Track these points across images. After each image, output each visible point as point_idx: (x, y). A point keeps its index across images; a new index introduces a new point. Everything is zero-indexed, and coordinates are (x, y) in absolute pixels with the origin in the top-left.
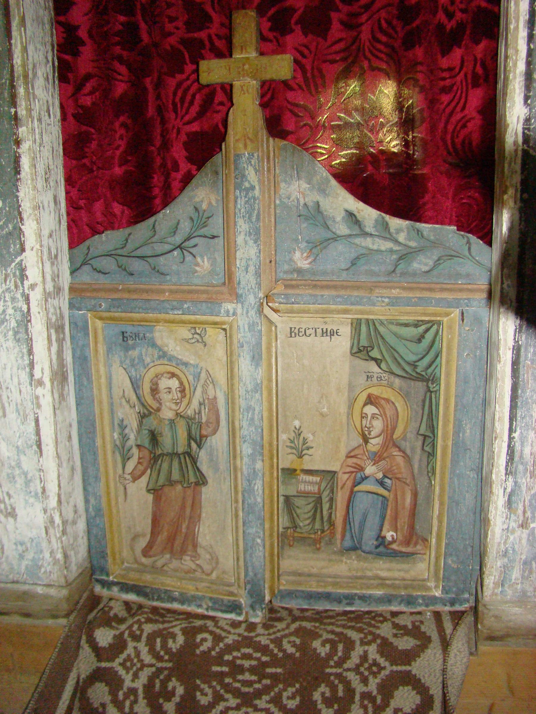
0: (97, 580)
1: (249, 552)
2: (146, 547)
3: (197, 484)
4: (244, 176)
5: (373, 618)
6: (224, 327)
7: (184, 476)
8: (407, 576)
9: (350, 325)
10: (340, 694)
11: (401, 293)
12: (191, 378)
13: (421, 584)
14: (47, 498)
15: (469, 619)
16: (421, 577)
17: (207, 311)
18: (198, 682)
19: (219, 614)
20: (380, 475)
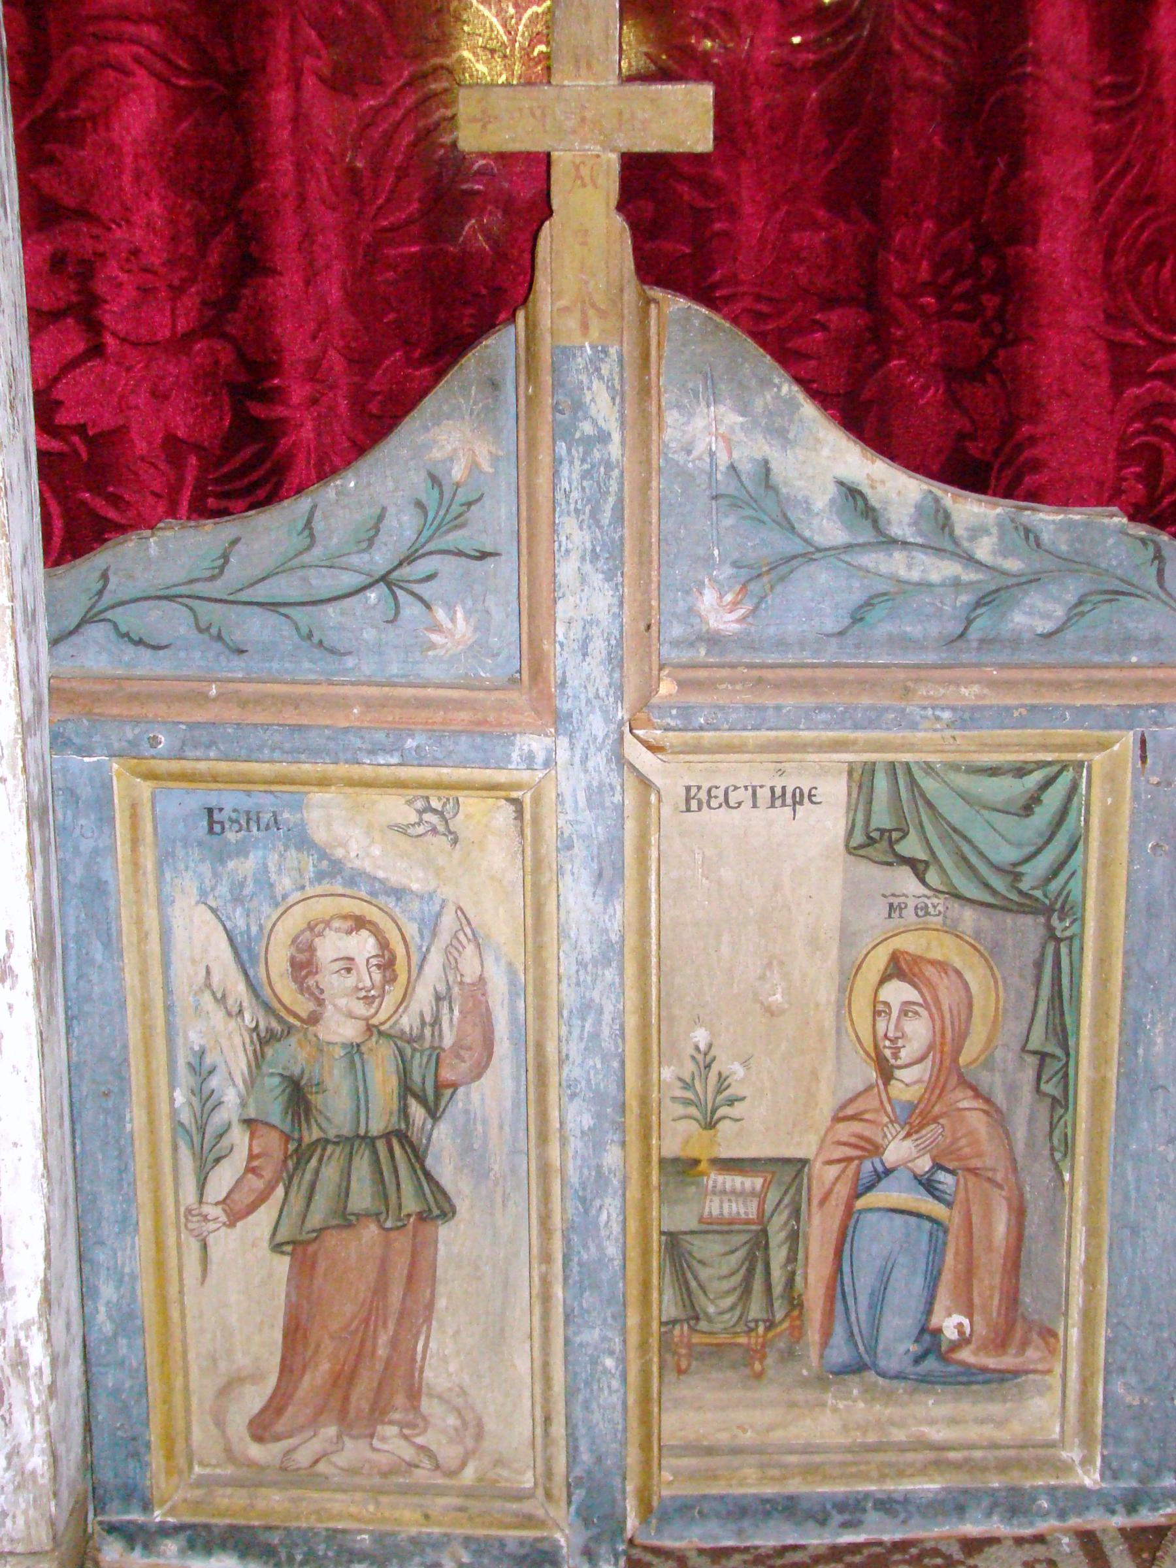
1: (581, 1398)
2: (263, 1410)
3: (424, 1217)
4: (578, 406)
6: (514, 795)
7: (386, 1197)
8: (1003, 1436)
9: (845, 775)
11: (983, 697)
12: (411, 929)
13: (1037, 1454)
16: (1039, 1437)
17: (472, 755)
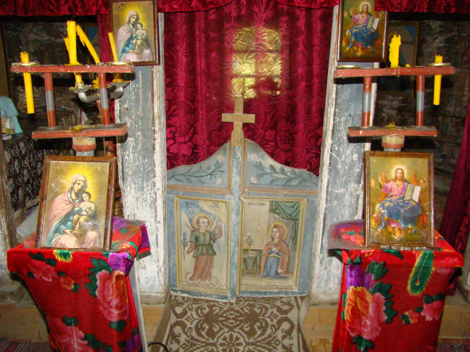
0: (172, 290)
3: (212, 255)
4: (236, 154)
5: (274, 299)
8: (286, 285)
10: (264, 325)
12: (212, 219)
13: (290, 287)
14: (159, 262)
15: (307, 299)
18: (214, 324)
19: (219, 300)
20: (277, 251)
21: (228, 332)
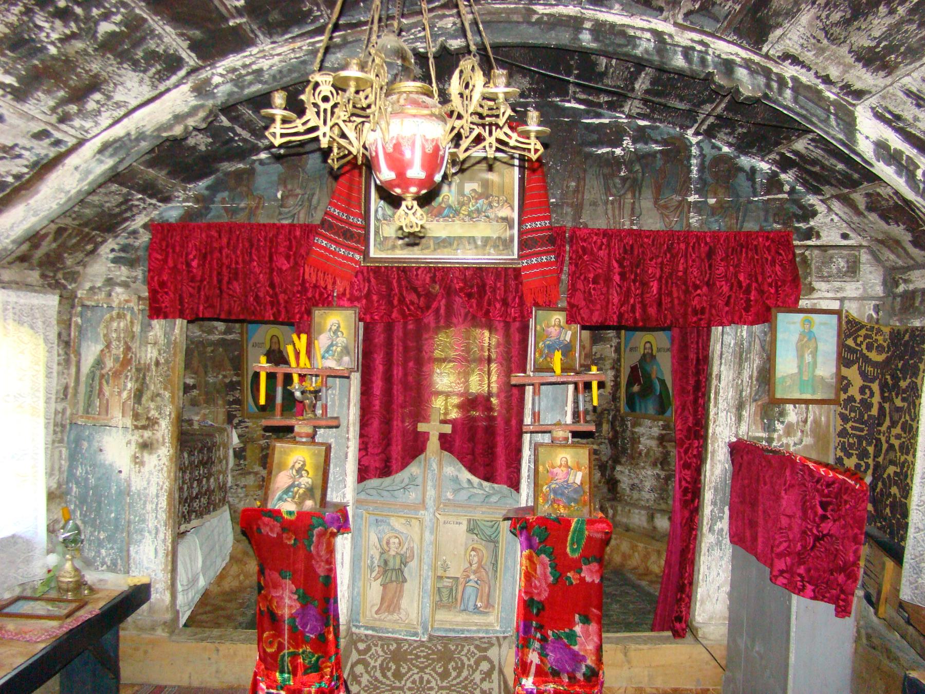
13: (491, 625)
21: (418, 673)
